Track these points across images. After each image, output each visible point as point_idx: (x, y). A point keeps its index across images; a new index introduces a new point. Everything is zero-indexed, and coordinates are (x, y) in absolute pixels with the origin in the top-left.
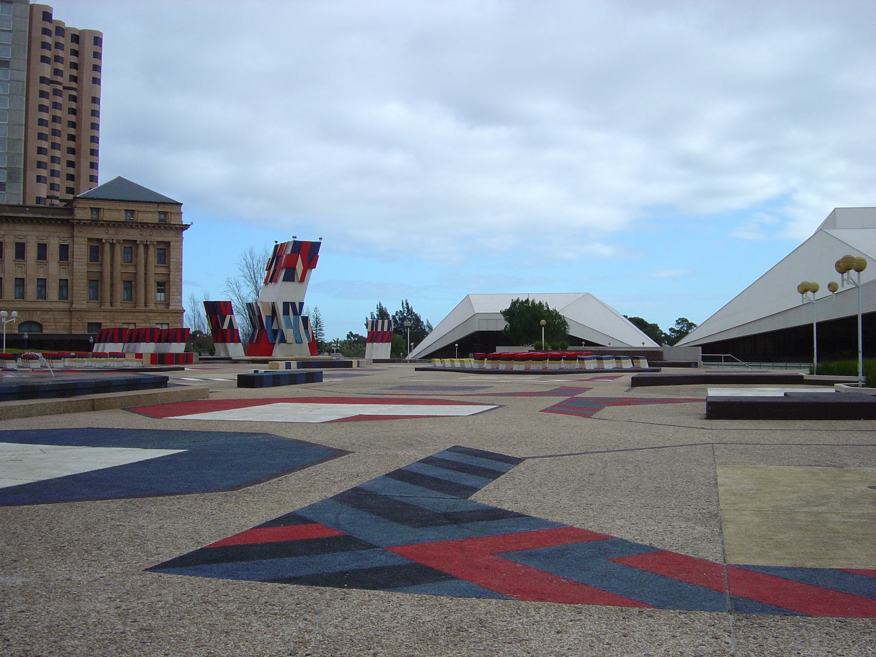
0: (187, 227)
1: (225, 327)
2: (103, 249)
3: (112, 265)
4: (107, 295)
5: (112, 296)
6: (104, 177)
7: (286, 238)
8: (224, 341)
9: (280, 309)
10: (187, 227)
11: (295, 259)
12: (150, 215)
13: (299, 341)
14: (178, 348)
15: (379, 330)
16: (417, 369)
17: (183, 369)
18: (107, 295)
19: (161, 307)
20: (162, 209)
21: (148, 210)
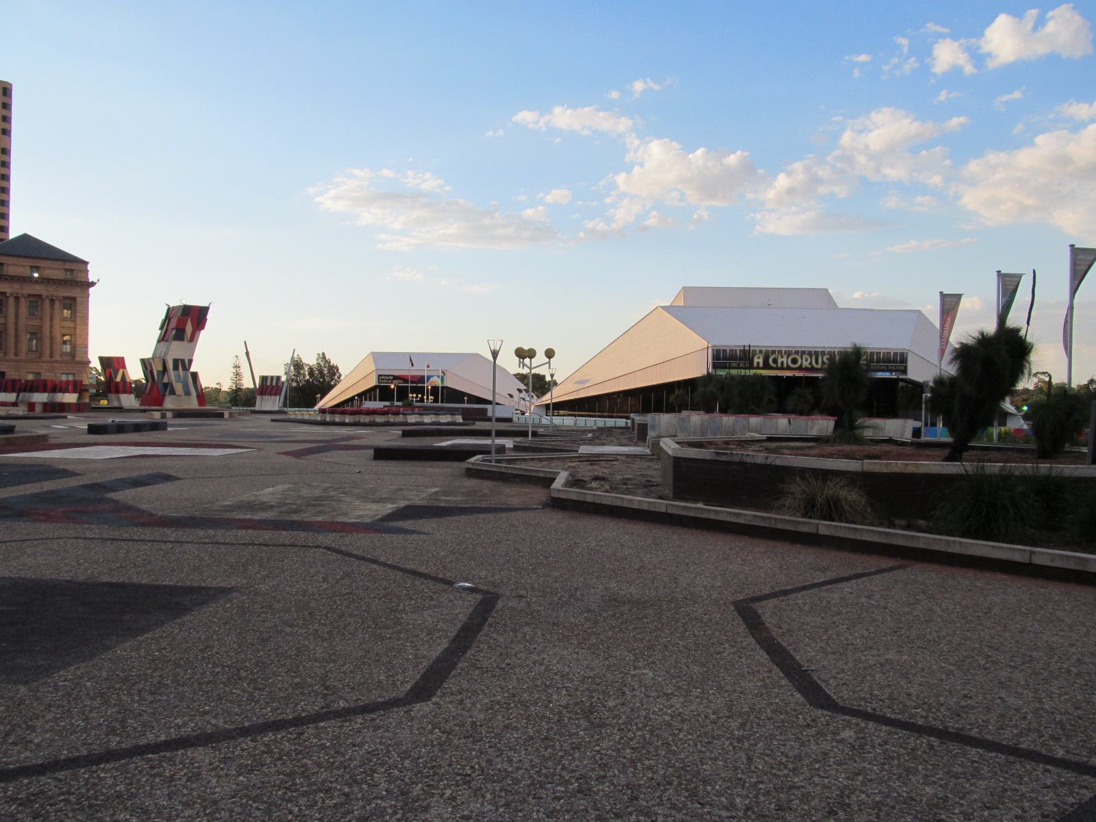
0: (93, 284)
1: (119, 379)
2: (7, 302)
3: (17, 317)
4: (12, 346)
5: (16, 347)
6: (14, 233)
7: (175, 303)
8: (117, 391)
9: (170, 365)
10: (93, 284)
11: (185, 322)
12: (56, 272)
13: (188, 393)
14: (70, 398)
15: (269, 384)
16: (272, 420)
17: (66, 417)
18: (12, 346)
19: (67, 358)
20: (68, 266)
21: (54, 267)
